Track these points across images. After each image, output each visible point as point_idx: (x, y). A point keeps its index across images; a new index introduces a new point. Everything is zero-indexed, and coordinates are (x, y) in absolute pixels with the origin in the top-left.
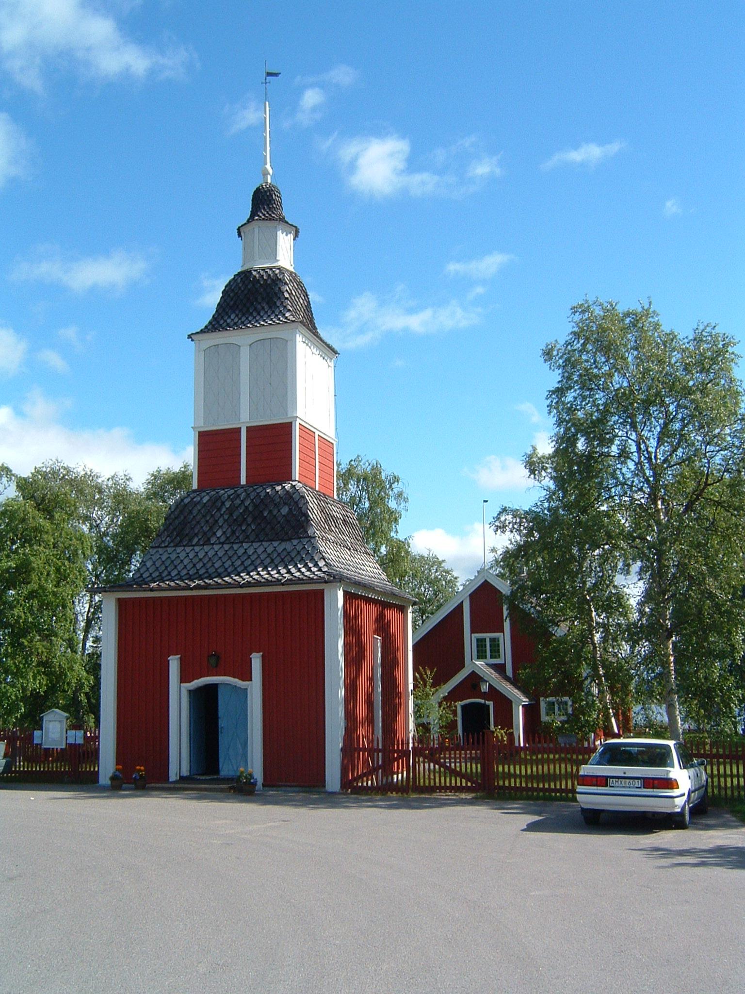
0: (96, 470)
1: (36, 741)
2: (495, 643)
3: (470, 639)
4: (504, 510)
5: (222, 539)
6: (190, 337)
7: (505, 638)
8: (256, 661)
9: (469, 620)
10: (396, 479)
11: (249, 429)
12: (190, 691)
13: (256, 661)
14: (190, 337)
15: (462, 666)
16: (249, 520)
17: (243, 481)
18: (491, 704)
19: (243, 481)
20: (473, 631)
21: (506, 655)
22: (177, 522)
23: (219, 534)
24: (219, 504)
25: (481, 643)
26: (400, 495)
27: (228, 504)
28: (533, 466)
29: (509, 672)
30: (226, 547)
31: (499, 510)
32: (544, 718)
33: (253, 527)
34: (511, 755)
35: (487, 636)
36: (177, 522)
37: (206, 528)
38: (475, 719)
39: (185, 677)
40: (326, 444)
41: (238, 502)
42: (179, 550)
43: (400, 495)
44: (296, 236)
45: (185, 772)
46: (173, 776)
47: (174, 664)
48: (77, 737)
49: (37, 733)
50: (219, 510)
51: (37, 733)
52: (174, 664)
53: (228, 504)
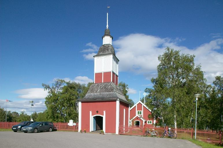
0: (80, 83)
3: (137, 112)
4: (147, 89)
6: (94, 56)
10: (127, 85)
11: (104, 73)
12: (93, 117)
14: (94, 56)
15: (135, 115)
17: (103, 82)
19: (103, 82)
20: (137, 110)
23: (98, 91)
25: (138, 112)
26: (128, 88)
27: (100, 86)
28: (153, 81)
29: (143, 117)
30: (100, 93)
32: (148, 124)
34: (210, 140)
35: (140, 111)
37: (96, 90)
38: (138, 124)
39: (92, 115)
40: (117, 76)
41: (102, 85)
42: (92, 93)
43: (128, 88)
44: (112, 39)
45: (92, 130)
46: (90, 131)
48: (75, 124)
49: (68, 123)
51: (68, 123)
53: (100, 86)
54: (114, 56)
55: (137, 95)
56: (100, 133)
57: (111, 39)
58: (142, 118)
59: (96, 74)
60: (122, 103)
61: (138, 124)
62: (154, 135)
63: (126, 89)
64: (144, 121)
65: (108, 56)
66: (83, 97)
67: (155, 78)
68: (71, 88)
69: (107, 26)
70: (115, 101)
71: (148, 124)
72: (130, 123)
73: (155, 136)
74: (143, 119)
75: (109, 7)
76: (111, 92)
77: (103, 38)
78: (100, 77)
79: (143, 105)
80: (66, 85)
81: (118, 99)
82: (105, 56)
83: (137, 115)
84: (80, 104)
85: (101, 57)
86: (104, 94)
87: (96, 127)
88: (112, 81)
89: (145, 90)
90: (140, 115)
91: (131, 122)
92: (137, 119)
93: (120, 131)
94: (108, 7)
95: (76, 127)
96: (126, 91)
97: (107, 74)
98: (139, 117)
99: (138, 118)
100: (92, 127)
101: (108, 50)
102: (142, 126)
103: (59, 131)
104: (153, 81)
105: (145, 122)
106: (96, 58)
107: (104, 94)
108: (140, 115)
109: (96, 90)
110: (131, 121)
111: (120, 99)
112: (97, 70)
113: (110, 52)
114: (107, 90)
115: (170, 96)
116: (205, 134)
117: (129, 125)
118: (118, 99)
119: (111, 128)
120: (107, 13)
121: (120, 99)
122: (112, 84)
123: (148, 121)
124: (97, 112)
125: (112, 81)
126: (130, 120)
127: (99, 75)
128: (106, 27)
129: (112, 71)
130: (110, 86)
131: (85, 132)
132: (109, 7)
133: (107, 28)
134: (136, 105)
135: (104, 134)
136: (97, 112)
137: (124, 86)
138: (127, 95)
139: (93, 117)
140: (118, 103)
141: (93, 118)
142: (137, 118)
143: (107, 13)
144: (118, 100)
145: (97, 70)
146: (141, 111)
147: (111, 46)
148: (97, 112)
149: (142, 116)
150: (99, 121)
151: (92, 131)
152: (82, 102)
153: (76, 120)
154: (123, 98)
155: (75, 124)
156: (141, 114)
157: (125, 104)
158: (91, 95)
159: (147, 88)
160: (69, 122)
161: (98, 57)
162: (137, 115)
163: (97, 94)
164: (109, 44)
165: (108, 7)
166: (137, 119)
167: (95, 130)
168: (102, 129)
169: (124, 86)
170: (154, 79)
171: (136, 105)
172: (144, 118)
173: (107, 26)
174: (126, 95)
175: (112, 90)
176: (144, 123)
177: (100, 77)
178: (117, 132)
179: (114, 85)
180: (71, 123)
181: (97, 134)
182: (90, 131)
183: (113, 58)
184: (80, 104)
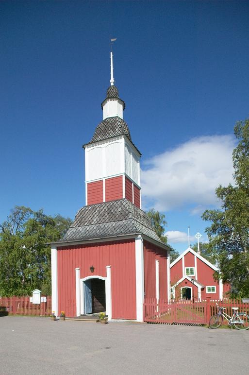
1: (31, 301)
2: (192, 270)
4: (207, 211)
5: (96, 223)
7: (195, 269)
8: (108, 270)
9: (87, 279)
12: (84, 282)
13: (108, 270)
15: (182, 277)
16: (106, 214)
17: (104, 201)
18: (191, 288)
19: (104, 201)
21: (196, 274)
22: (79, 217)
24: (95, 209)
25: (188, 270)
26: (164, 222)
27: (98, 209)
29: (196, 279)
30: (97, 225)
31: (205, 211)
32: (207, 292)
33: (107, 217)
35: (190, 268)
36: (79, 217)
37: (90, 219)
38: (187, 294)
39: (82, 277)
45: (82, 313)
46: (78, 315)
47: (77, 272)
48: (44, 299)
49: (31, 298)
50: (95, 211)
51: (31, 298)
52: (77, 272)
53: (98, 209)
54: (129, 142)
55: (186, 238)
56: (98, 321)
57: (121, 106)
58: (196, 281)
59: (89, 184)
60: (149, 245)
61: (187, 294)
62: (235, 324)
63: (162, 225)
64: (200, 287)
65: (114, 142)
66: (59, 236)
67: (226, 187)
68: (45, 223)
69: (112, 80)
70: (133, 240)
71: (207, 292)
72: (171, 292)
73: (239, 325)
74: (198, 283)
75: (115, 40)
76: (124, 221)
77: (104, 107)
78: (99, 190)
79: (197, 255)
80: (32, 217)
81: (140, 236)
82: (108, 143)
83: (185, 276)
84: (54, 252)
85: (100, 146)
86: (106, 226)
87: (91, 304)
88: (124, 197)
89: (204, 215)
90: (190, 275)
91: (174, 291)
92: (186, 283)
93: (146, 314)
94: (112, 40)
95: (48, 305)
96: (161, 227)
97: (113, 182)
98: (190, 280)
99: (188, 283)
100: (81, 306)
101: (114, 130)
102: (196, 297)
103: (13, 314)
104: (221, 192)
105: (203, 289)
106: (90, 149)
107: (106, 226)
108: (190, 275)
109: (90, 219)
110: (173, 287)
111: (143, 235)
112: (90, 176)
113: (118, 131)
114: (112, 216)
115: (228, 261)
116: (148, 307)
117: (169, 298)
118: (140, 236)
119: (125, 309)
120: (111, 53)
121: (143, 235)
122: (124, 204)
123: (207, 287)
124: (92, 269)
125: (126, 197)
126: (171, 286)
127: (96, 186)
128: (110, 83)
129: (125, 174)
130: (120, 208)
131: (62, 318)
132: (115, 40)
133: (112, 84)
134: (182, 256)
135: (107, 323)
136: (91, 268)
137: (157, 218)
138: (164, 236)
139: (84, 282)
140: (139, 244)
141: (82, 283)
142: (186, 282)
143: (111, 53)
144: (140, 238)
145: (90, 176)
146: (194, 268)
147: (120, 120)
148: (92, 269)
149: (194, 277)
150: (96, 288)
151: (81, 315)
152: (58, 249)
153: (47, 293)
154: (153, 235)
155: (44, 299)
156: (192, 273)
157: (158, 250)
158: (78, 232)
159: (209, 209)
160: (30, 294)
161: (92, 148)
162: (185, 276)
163: (91, 228)
164: (117, 117)
165: (112, 40)
166: (186, 283)
167: (90, 311)
168: (104, 310)
169: (157, 218)
170: (225, 188)
171: (182, 256)
172: (199, 282)
173: (112, 80)
174: (162, 236)
175: (125, 215)
176: (200, 291)
177: (99, 190)
178: (140, 317)
179: (129, 206)
180: (36, 297)
181: (91, 325)
182: (78, 315)
183: (126, 145)
184: (54, 252)
